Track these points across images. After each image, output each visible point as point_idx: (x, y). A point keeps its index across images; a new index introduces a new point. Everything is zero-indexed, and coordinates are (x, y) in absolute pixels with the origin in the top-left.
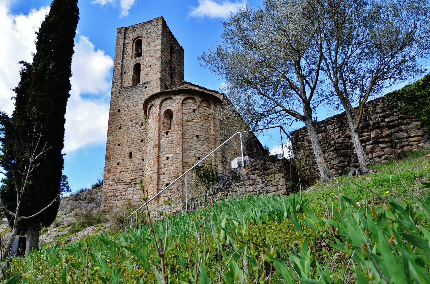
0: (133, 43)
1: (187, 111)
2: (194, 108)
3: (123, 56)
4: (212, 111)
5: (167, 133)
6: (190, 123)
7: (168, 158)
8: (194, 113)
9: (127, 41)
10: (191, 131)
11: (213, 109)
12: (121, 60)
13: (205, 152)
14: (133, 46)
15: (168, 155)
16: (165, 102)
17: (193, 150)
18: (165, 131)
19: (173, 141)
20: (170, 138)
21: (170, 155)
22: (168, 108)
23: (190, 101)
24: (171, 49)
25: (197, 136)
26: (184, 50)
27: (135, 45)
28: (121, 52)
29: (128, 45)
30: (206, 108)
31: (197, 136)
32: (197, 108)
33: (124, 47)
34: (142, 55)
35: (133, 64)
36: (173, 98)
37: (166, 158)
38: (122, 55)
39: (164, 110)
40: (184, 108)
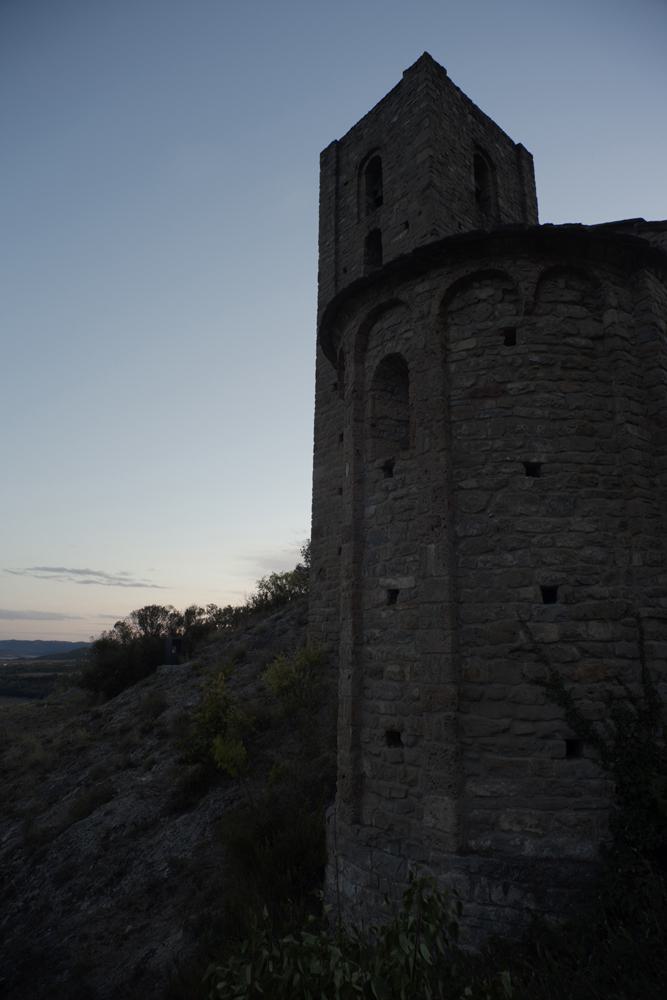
0: (359, 175)
1: (471, 343)
2: (504, 323)
3: (336, 225)
4: (609, 316)
5: (388, 469)
6: (490, 403)
7: (393, 594)
8: (506, 351)
9: (343, 178)
10: (499, 444)
11: (619, 308)
12: (333, 238)
13: (588, 551)
14: (359, 186)
15: (391, 582)
16: (378, 326)
17: (513, 550)
18: (380, 462)
19: (411, 509)
20: (401, 492)
21: (404, 583)
22: (391, 348)
23: (483, 294)
24: (476, 156)
25: (532, 470)
26: (531, 156)
27: (364, 178)
28: (332, 216)
29: (348, 187)
30: (578, 310)
31: (532, 470)
32: (520, 319)
33: (338, 197)
34: (384, 202)
35: (363, 238)
36: (404, 296)
37: (384, 596)
38: (333, 223)
39: (373, 362)
40: (453, 332)
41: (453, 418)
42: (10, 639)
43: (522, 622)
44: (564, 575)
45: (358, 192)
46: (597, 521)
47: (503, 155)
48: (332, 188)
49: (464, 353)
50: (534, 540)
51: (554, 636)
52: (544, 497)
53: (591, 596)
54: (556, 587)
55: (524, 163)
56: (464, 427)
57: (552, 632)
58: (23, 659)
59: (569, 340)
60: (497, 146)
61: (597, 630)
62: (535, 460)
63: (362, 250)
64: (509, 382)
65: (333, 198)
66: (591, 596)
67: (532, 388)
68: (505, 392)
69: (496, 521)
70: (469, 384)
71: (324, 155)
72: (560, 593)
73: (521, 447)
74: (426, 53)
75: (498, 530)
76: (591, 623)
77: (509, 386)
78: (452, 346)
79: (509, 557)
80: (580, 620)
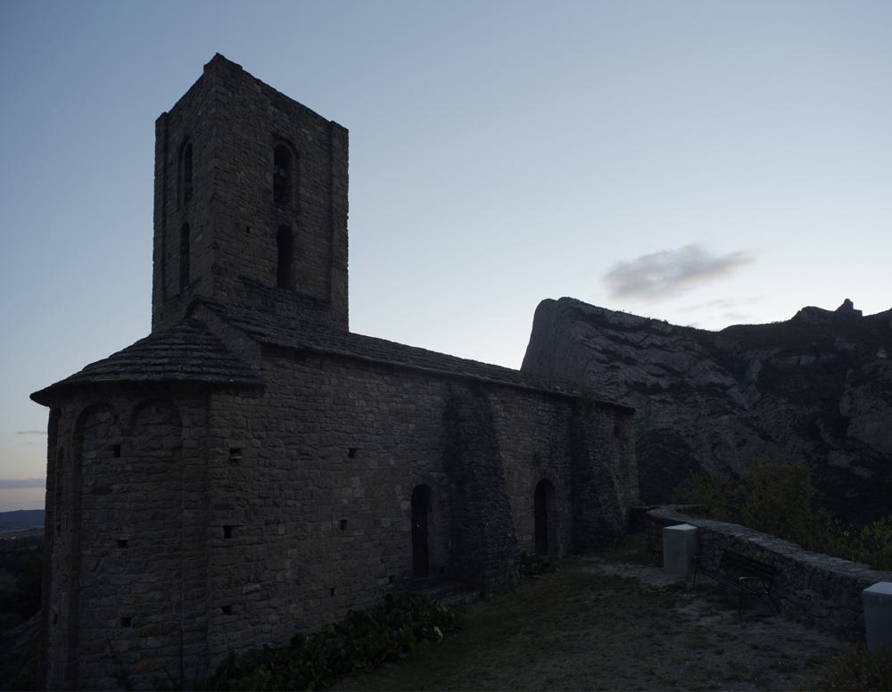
14: (179, 171)
17: (107, 596)
25: (123, 544)
41: (83, 507)
42: (19, 509)
43: (109, 640)
44: (134, 611)
45: (179, 177)
46: (159, 575)
47: (310, 139)
48: (162, 165)
49: (90, 461)
50: (119, 590)
51: (126, 649)
52: (128, 562)
53: (150, 622)
54: (130, 618)
55: (336, 143)
56: (88, 514)
57: (123, 645)
58: (35, 529)
59: (153, 453)
60: (304, 130)
61: (152, 642)
62: (123, 539)
63: (179, 239)
64: (113, 484)
65: (162, 176)
66: (150, 622)
67: (126, 489)
68: (111, 491)
69: (99, 577)
70: (91, 484)
71: (158, 122)
72: (132, 622)
73: (116, 530)
74: (218, 54)
75: (101, 583)
76: (149, 638)
77: (113, 487)
78: (84, 455)
79: (105, 600)
80: (142, 637)
